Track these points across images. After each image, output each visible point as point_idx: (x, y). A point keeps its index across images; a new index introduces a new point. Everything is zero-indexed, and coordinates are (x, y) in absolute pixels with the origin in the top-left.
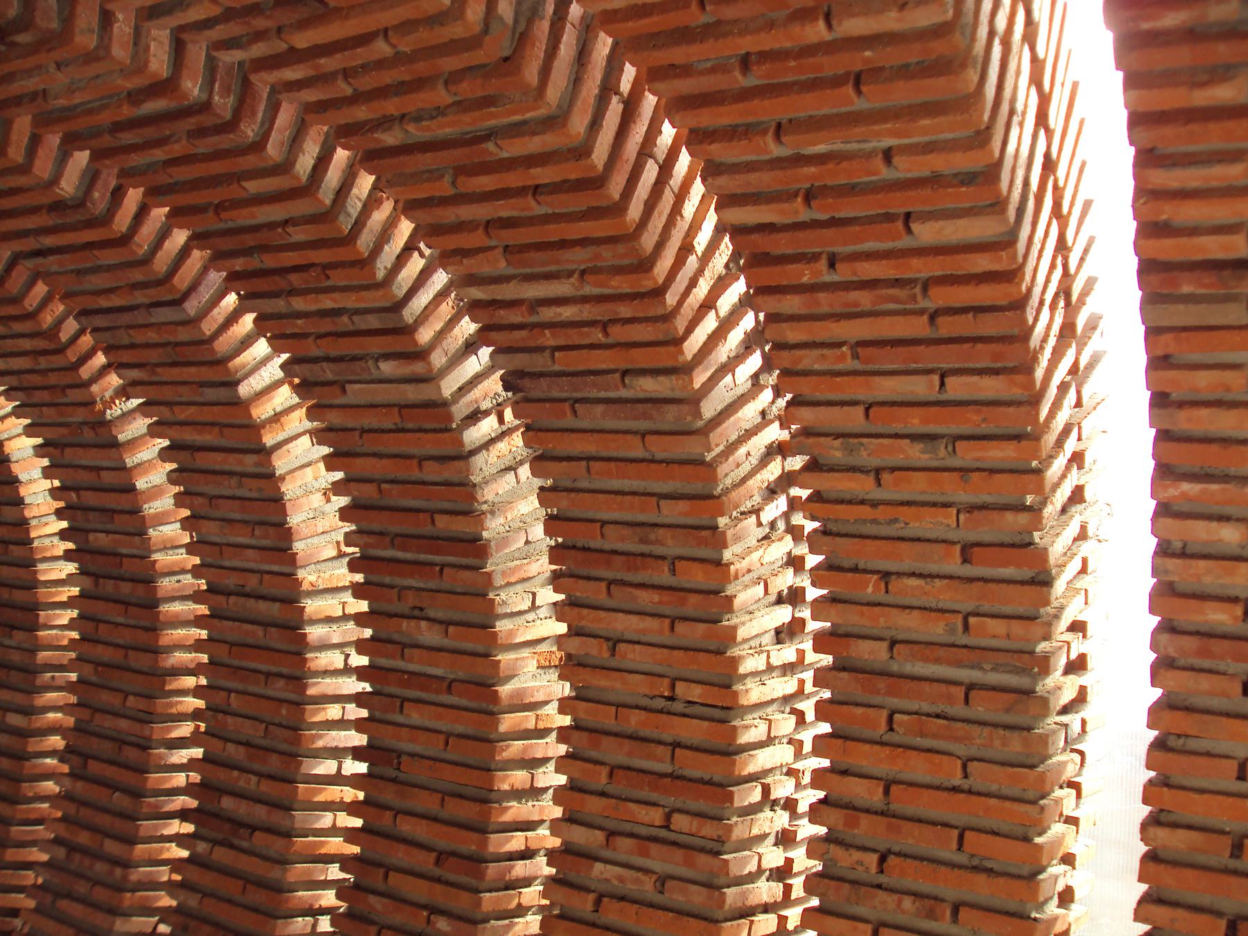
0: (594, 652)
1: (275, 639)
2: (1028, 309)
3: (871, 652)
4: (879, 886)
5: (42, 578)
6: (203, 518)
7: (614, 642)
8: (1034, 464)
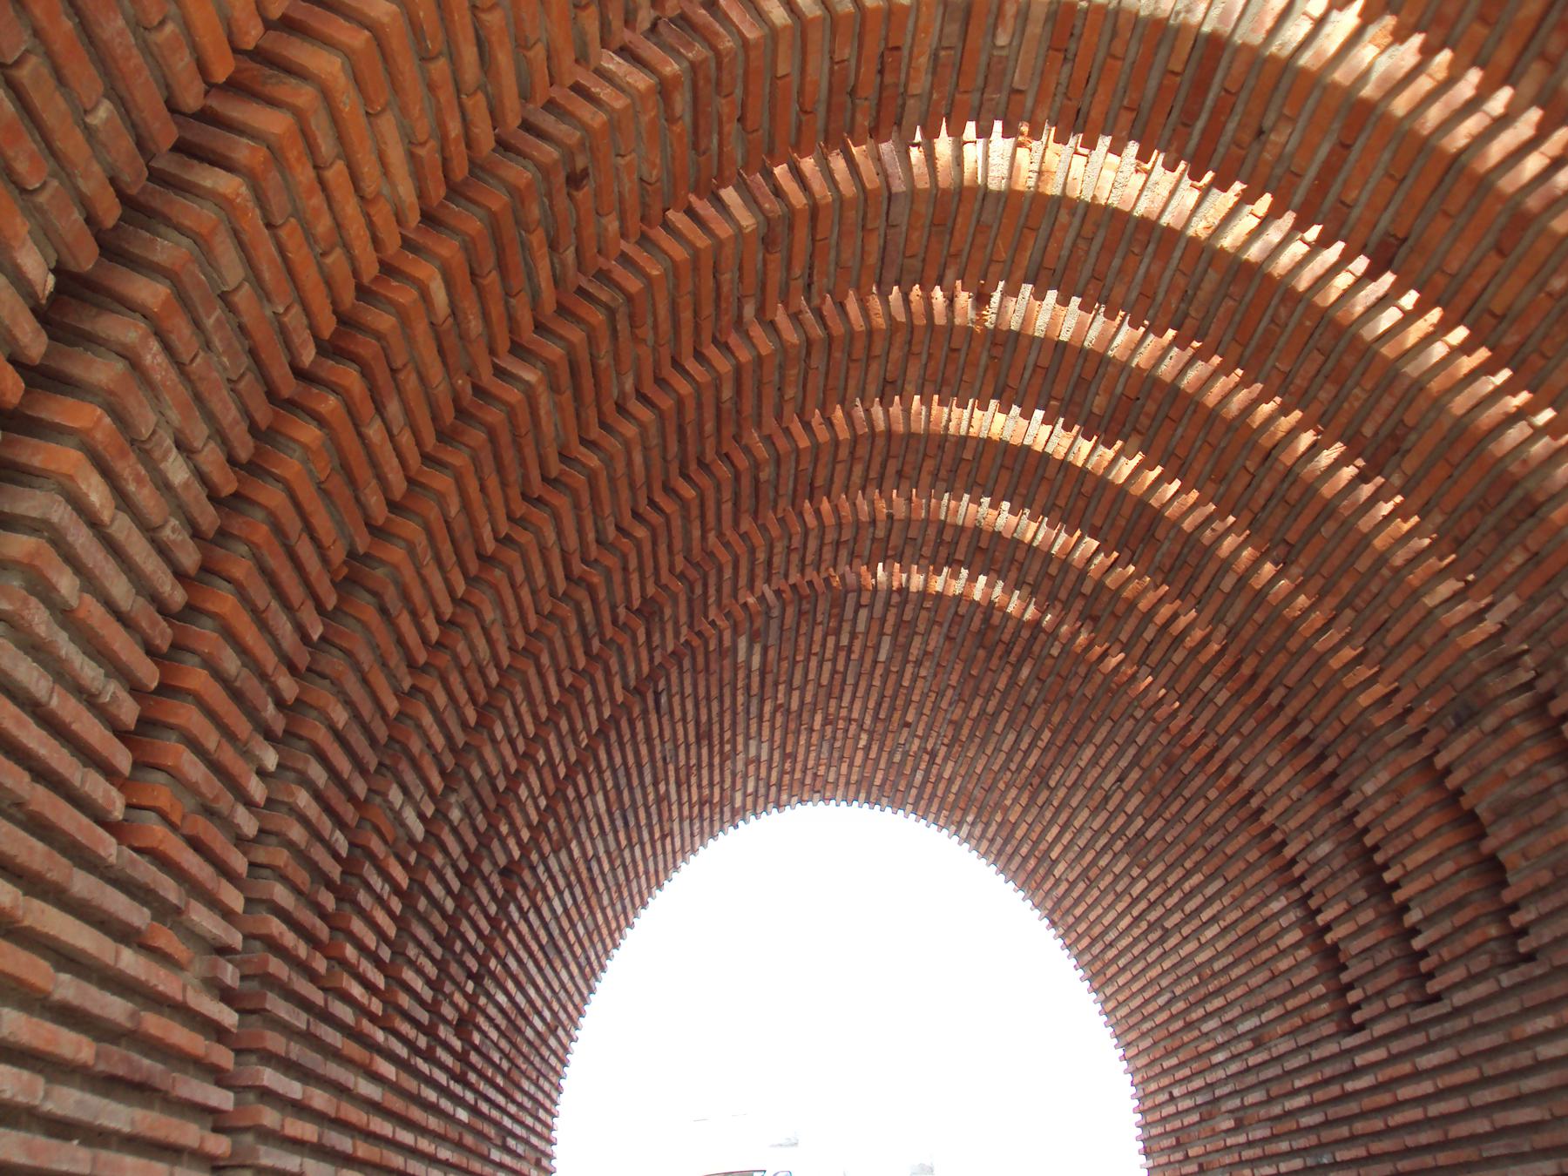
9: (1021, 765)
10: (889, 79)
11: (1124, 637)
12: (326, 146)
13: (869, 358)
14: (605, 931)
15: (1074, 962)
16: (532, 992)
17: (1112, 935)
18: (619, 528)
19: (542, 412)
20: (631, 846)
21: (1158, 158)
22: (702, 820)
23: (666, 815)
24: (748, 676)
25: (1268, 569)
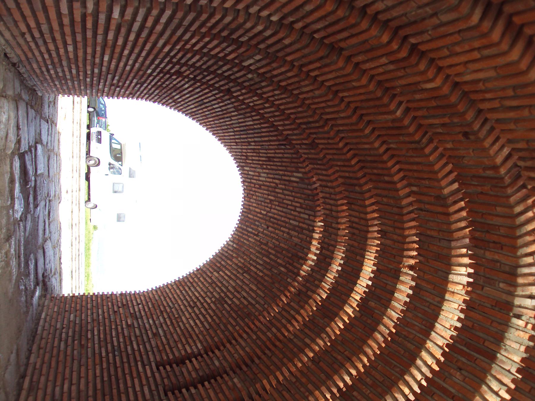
5: (345, 308)
9: (251, 265)
10: (491, 245)
11: (292, 304)
12: (486, 52)
13: (395, 228)
14: (206, 121)
15: (185, 276)
16: (188, 96)
17: (193, 289)
18: (343, 138)
19: (386, 116)
20: (234, 132)
21: (455, 334)
22: (241, 156)
23: (244, 144)
24: (288, 176)
25: (311, 355)
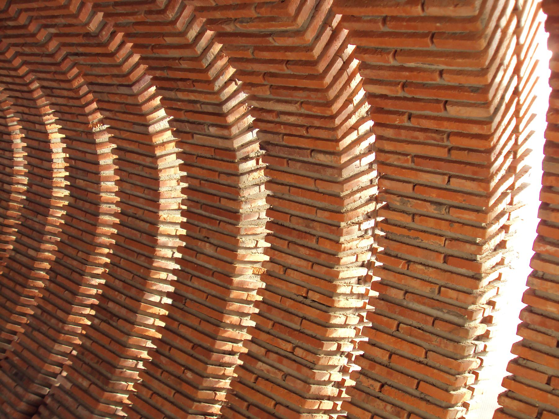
0: (277, 271)
1: (144, 239)
2: (492, 154)
3: (396, 294)
4: (378, 398)
5: (54, 195)
6: (125, 181)
7: (286, 268)
8: (483, 224)
